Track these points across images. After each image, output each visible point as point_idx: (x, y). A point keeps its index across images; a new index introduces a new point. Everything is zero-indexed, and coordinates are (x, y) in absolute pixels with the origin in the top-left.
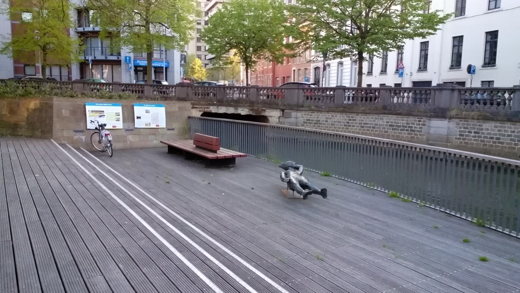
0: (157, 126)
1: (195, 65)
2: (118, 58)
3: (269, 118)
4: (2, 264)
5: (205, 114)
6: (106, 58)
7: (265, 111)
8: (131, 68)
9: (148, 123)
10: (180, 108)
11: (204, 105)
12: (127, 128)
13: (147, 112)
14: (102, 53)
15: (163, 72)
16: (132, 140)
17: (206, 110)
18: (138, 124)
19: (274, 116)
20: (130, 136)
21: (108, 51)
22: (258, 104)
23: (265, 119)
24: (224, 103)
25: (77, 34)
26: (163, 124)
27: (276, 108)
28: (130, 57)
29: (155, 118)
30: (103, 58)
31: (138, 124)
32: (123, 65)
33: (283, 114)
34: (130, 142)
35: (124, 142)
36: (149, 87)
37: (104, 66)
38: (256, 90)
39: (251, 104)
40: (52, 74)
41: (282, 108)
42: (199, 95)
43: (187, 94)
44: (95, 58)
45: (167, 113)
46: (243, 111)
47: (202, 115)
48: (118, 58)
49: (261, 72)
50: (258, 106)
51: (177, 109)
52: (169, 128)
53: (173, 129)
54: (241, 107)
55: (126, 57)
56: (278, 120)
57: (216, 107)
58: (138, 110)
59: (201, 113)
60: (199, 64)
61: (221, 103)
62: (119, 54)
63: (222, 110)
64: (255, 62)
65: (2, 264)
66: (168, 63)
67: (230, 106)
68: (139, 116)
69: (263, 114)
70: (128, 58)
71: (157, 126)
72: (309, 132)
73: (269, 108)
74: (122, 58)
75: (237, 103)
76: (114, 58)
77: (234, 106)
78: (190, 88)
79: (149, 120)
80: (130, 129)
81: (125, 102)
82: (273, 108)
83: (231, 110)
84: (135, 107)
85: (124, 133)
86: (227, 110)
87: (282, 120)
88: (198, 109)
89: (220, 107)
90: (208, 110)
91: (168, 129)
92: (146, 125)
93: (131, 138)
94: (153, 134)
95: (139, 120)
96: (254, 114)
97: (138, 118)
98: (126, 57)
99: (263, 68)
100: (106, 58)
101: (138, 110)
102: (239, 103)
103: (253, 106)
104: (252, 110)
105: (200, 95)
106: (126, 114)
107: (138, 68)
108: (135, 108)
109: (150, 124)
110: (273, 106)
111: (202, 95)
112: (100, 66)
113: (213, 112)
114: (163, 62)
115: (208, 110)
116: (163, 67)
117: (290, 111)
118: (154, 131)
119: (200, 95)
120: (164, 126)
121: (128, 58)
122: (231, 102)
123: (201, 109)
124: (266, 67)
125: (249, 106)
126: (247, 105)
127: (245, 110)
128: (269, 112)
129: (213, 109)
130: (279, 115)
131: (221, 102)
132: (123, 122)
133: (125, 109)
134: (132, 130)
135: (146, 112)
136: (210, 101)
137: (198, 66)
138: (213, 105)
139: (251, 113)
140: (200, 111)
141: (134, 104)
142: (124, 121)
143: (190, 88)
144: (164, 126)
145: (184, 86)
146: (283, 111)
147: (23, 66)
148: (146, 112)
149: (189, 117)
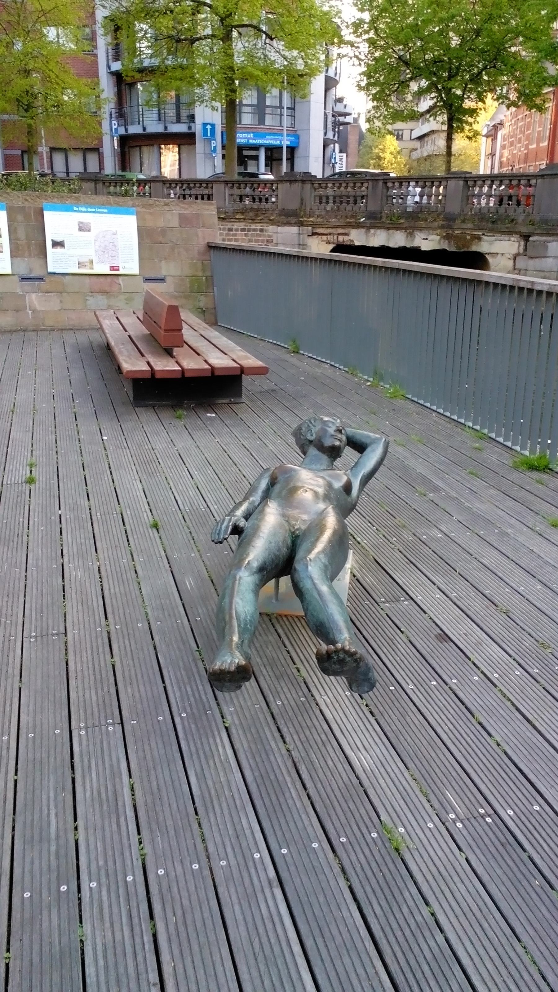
0: (112, 268)
1: (383, 151)
2: (190, 128)
3: (490, 260)
4: (3, 537)
5: (339, 248)
6: (166, 128)
7: (479, 238)
8: (215, 150)
9: (85, 259)
10: (184, 220)
11: (336, 227)
12: (24, 273)
13: (83, 228)
14: (160, 120)
15: (282, 160)
16: (38, 308)
17: (341, 238)
18: (56, 262)
19: (501, 252)
20: (34, 296)
21: (171, 114)
22: (463, 221)
23: (478, 260)
24: (384, 220)
25: (110, 76)
26: (131, 265)
27: (510, 233)
28: (213, 125)
29: (108, 248)
30: (159, 129)
31: (56, 262)
32: (199, 145)
33: (525, 250)
34: (34, 311)
35: (17, 311)
36: (222, 186)
37: (163, 146)
38: (461, 183)
39: (447, 222)
40: (70, 170)
41: (524, 230)
42: (327, 203)
43: (302, 200)
44: (144, 129)
45: (144, 234)
46: (427, 242)
47: (333, 251)
48: (190, 128)
49: (522, 157)
50: (464, 226)
51: (175, 223)
52: (148, 276)
53: (162, 280)
54: (421, 229)
55: (205, 125)
56: (511, 263)
57: (363, 230)
58: (58, 222)
59: (331, 246)
60: (392, 149)
61: (375, 221)
62: (192, 118)
63: (378, 239)
64: (473, 112)
65: (3, 537)
66: (298, 137)
67: (397, 229)
68: (58, 239)
69: (474, 248)
70: (209, 127)
71: (112, 268)
72: (496, 285)
73: (491, 230)
74: (198, 128)
75: (413, 220)
76: (181, 128)
77: (405, 229)
78: (308, 186)
79: (89, 253)
80: (32, 275)
81: (18, 198)
82: (502, 233)
83: (398, 240)
84: (46, 213)
85: (18, 288)
86: (388, 240)
87: (521, 263)
88: (325, 238)
89: (372, 231)
90: (346, 238)
91: (147, 280)
92: (81, 265)
93: (35, 299)
94: (102, 292)
95: (59, 250)
96: (453, 249)
97: (55, 244)
98: (205, 125)
99: (527, 147)
100: (166, 128)
101: (58, 222)
102: (418, 219)
103: (450, 227)
104: (448, 237)
105: (331, 201)
106: (21, 234)
107: (245, 153)
108: (49, 217)
109: (91, 262)
110: (497, 224)
111: (334, 202)
112: (156, 147)
113: (357, 243)
114: (282, 135)
115: (346, 238)
116: (281, 148)
117: (544, 238)
118: (107, 283)
119: (331, 201)
120: (135, 270)
121: (209, 127)
122: (400, 217)
123: (330, 238)
124: (534, 146)
125: (442, 227)
126: (436, 224)
127: (431, 237)
128: (491, 243)
129: (357, 237)
130: (515, 251)
131: (375, 218)
132: (12, 256)
133: (20, 218)
134: (40, 279)
135: (81, 229)
136: (352, 216)
137: (391, 153)
138: (358, 226)
139: (445, 246)
140: (328, 242)
141: (45, 204)
142: (14, 254)
143: (308, 186)
144: (135, 270)
145: (296, 181)
146: (526, 237)
147: (19, 153)
148: (81, 229)
149: (211, 247)
